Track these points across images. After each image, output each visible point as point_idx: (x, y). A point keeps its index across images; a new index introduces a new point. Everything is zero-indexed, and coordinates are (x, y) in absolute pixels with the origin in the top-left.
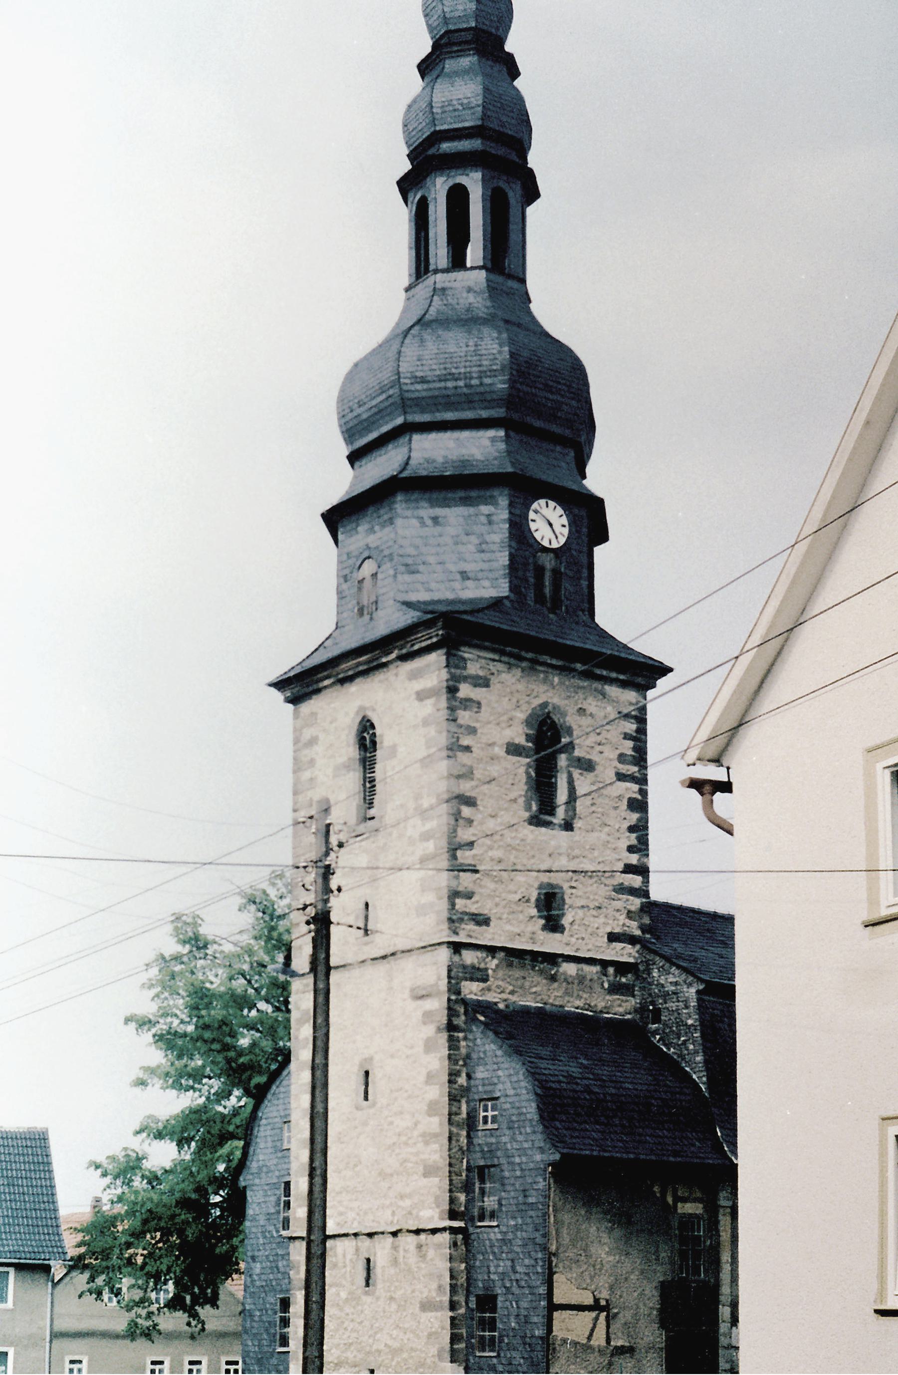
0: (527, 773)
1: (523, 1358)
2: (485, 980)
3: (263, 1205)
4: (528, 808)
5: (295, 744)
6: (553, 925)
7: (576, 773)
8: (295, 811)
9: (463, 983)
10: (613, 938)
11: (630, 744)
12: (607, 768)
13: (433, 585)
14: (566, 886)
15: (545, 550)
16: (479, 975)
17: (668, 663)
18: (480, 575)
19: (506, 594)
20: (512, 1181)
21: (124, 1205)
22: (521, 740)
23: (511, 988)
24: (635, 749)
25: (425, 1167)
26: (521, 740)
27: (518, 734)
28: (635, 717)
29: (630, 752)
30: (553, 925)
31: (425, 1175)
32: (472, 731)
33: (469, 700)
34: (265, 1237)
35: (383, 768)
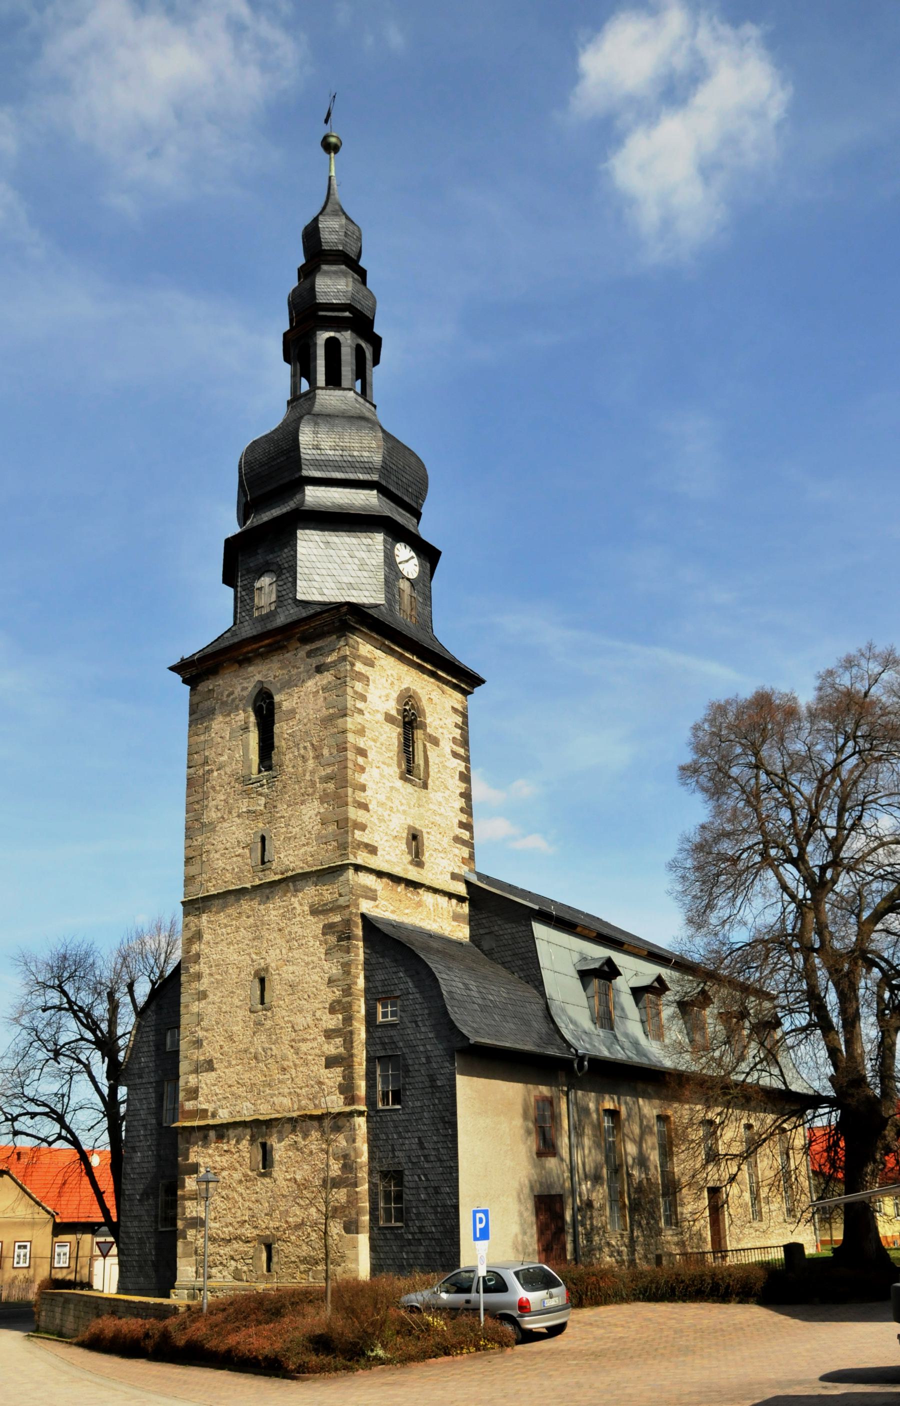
0: (399, 739)
1: (435, 1226)
2: (374, 899)
3: (144, 1102)
4: (399, 766)
5: (190, 715)
6: (418, 861)
7: (428, 745)
8: (189, 767)
9: (361, 899)
10: (454, 877)
11: (459, 731)
12: (447, 746)
13: (325, 591)
14: (424, 831)
15: (404, 577)
16: (370, 894)
17: (482, 675)
18: (362, 587)
19: (383, 602)
20: (416, 1067)
21: (785, 854)
22: (394, 713)
23: (392, 908)
24: (462, 735)
25: (326, 1059)
26: (394, 713)
27: (392, 707)
28: (461, 713)
29: (459, 737)
30: (418, 861)
31: (327, 1066)
32: (363, 698)
33: (360, 673)
34: (146, 1130)
35: (281, 729)
